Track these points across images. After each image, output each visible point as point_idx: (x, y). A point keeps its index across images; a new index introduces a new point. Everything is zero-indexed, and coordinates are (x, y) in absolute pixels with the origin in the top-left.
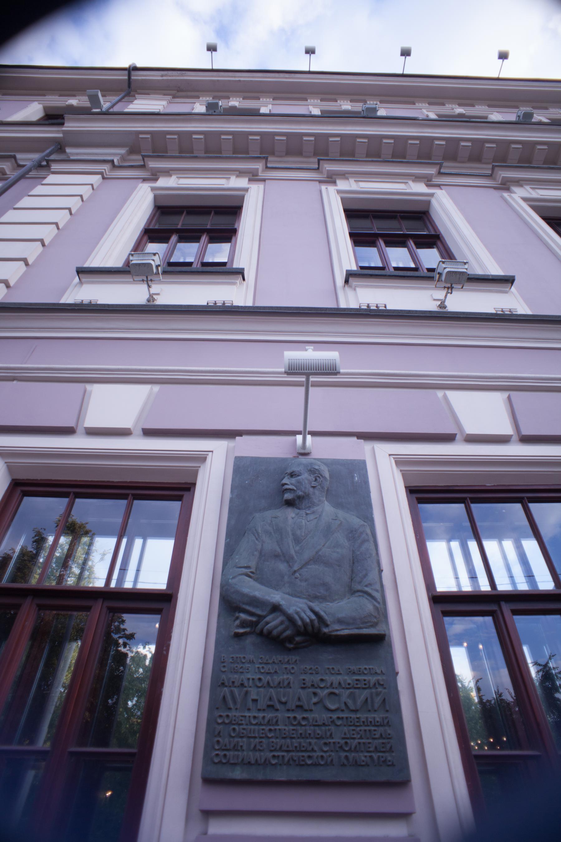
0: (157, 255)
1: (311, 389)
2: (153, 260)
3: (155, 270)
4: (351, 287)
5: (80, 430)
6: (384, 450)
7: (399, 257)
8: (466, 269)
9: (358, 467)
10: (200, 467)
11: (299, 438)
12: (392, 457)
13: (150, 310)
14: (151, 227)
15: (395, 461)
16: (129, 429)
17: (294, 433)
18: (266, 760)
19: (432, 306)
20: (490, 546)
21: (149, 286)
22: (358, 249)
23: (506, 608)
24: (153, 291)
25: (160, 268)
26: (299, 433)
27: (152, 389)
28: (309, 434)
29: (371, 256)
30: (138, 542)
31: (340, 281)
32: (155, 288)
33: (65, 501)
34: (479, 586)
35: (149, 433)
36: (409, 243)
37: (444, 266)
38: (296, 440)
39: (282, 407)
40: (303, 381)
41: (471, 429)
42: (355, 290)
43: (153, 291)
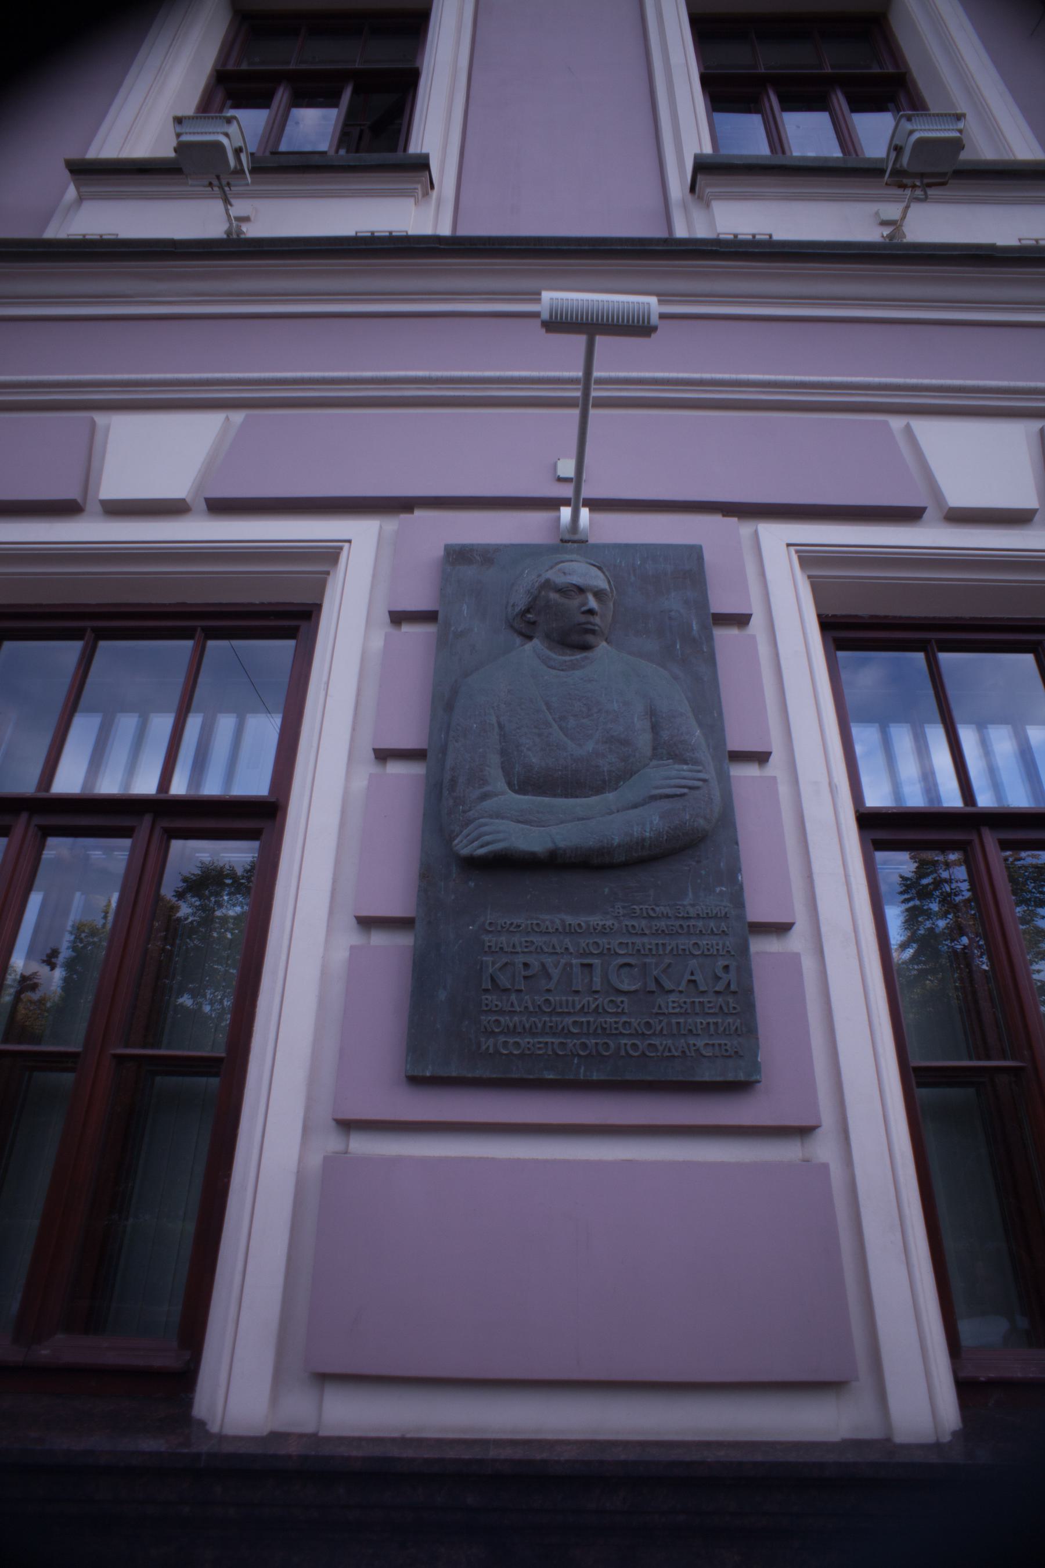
0: (235, 123)
1: (592, 412)
2: (227, 135)
3: (232, 162)
4: (700, 198)
5: (92, 506)
6: (777, 538)
7: (809, 134)
8: (960, 131)
9: (687, 568)
10: (328, 573)
11: (566, 513)
12: (792, 549)
13: (235, 250)
14: (230, 66)
15: (800, 558)
16: (183, 501)
17: (553, 504)
18: (563, 1028)
19: (874, 235)
20: (968, 737)
21: (227, 201)
22: (719, 117)
23: (990, 838)
24: (234, 212)
25: (243, 156)
26: (566, 502)
27: (227, 418)
28: (584, 505)
29: (748, 136)
30: (226, 724)
31: (677, 188)
32: (240, 207)
33: (78, 645)
34: (938, 798)
35: (222, 507)
36: (834, 97)
37: (909, 126)
38: (559, 518)
39: (525, 451)
40: (578, 398)
41: (957, 498)
42: (708, 206)
43: (234, 212)
